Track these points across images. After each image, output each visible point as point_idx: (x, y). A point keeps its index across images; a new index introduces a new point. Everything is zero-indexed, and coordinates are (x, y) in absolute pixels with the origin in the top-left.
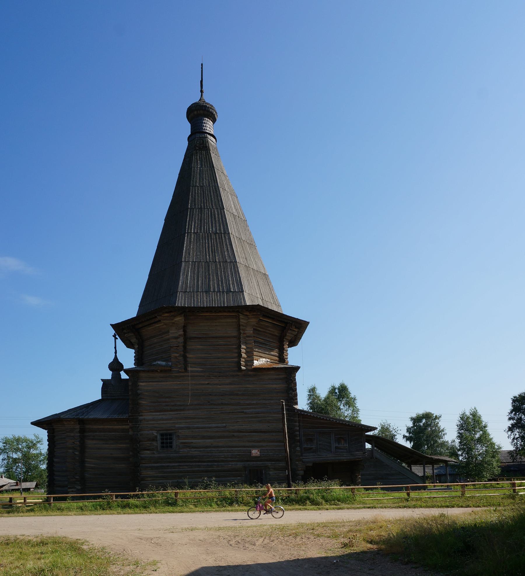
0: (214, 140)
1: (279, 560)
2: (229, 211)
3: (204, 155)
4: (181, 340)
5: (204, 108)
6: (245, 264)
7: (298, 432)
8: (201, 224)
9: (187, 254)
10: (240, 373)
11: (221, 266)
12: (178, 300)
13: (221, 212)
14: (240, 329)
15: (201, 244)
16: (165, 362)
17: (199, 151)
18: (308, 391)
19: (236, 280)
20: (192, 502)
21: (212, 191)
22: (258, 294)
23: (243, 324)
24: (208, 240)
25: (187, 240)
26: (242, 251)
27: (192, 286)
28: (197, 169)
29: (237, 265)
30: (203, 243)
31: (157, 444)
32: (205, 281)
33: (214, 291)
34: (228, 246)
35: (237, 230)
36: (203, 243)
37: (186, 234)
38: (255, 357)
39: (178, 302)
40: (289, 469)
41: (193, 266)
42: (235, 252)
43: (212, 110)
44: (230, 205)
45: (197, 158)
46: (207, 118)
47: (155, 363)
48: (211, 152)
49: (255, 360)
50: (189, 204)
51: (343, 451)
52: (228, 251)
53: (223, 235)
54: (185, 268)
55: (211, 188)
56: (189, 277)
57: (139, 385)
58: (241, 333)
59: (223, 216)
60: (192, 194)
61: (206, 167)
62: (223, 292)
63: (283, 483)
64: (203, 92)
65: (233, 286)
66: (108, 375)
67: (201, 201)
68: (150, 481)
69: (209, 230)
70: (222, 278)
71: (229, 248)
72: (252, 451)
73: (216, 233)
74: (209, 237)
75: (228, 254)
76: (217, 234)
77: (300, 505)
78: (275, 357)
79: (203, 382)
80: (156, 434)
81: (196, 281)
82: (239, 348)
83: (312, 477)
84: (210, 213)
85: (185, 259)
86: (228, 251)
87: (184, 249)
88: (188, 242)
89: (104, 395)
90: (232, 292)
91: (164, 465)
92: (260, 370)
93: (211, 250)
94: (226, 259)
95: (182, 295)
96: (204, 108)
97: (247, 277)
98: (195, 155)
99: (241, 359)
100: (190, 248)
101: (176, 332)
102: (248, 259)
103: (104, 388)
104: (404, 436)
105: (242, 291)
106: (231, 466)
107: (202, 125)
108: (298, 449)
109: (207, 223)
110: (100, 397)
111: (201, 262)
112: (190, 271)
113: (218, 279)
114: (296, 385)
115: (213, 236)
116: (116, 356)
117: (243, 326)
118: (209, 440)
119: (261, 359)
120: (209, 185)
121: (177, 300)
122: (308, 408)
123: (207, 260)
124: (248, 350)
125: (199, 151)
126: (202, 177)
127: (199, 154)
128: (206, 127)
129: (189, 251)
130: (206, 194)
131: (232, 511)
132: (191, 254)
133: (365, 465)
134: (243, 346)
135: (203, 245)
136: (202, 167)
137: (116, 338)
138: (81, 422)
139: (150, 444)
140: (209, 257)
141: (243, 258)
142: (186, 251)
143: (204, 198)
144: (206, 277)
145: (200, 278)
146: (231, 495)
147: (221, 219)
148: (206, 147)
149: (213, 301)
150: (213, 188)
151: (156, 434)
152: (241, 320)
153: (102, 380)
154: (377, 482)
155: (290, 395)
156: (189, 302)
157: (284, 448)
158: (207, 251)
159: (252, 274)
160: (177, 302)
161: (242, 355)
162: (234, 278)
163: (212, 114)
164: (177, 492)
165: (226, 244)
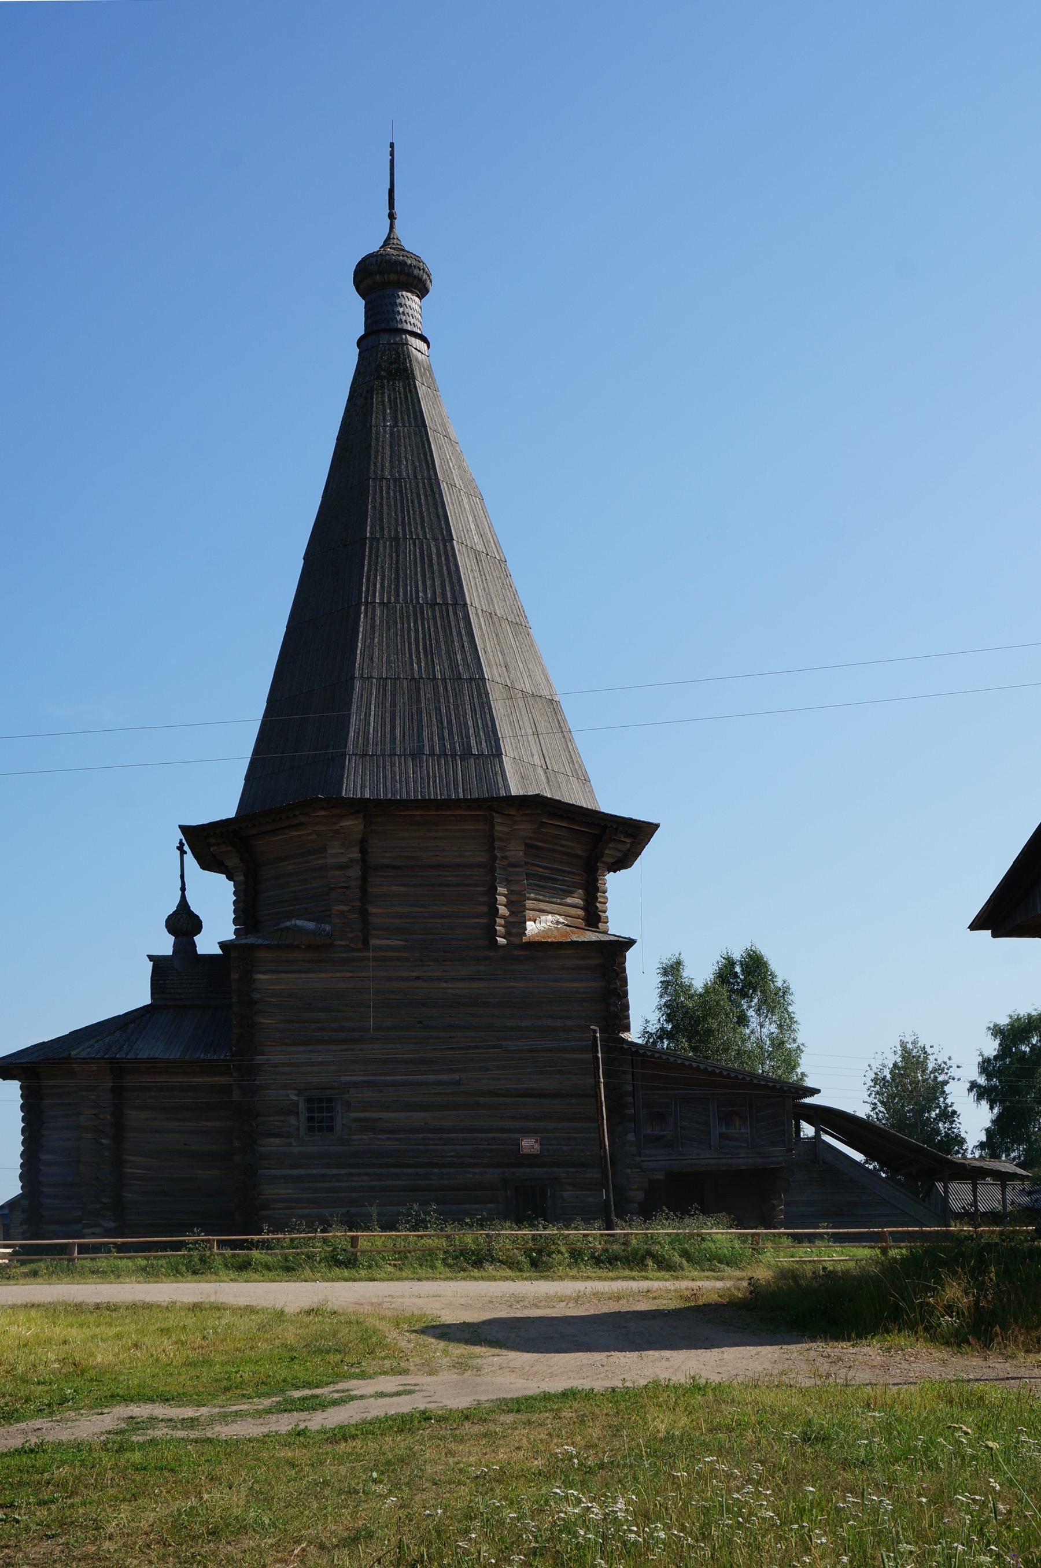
0: (422, 346)
1: (594, 1313)
2: (464, 542)
3: (400, 394)
4: (355, 872)
5: (399, 268)
6: (503, 682)
7: (632, 1098)
8: (397, 579)
9: (367, 660)
10: (492, 954)
11: (447, 690)
12: (347, 776)
13: (445, 547)
14: (494, 848)
15: (399, 632)
16: (314, 923)
17: (388, 382)
18: (661, 971)
19: (483, 725)
20: (389, 1260)
21: (422, 492)
22: (536, 757)
23: (501, 835)
24: (416, 623)
25: (365, 622)
26: (497, 646)
27: (379, 739)
28: (385, 431)
29: (485, 686)
30: (403, 631)
31: (298, 1122)
32: (411, 728)
33: (432, 754)
34: (465, 638)
35: (485, 591)
36: (403, 631)
37: (363, 608)
38: (529, 914)
39: (347, 781)
40: (608, 1186)
41: (381, 690)
42: (480, 654)
43: (420, 270)
44: (465, 524)
45: (383, 402)
46: (407, 291)
47: (288, 924)
48: (417, 382)
49: (530, 920)
50: (368, 528)
51: (738, 1144)
52: (463, 652)
53: (450, 608)
54: (362, 695)
55: (421, 485)
56: (372, 719)
57: (254, 980)
58: (497, 857)
59: (451, 558)
60: (374, 500)
61: (407, 425)
62: (454, 756)
63: (595, 1219)
64: (395, 219)
65: (476, 742)
66: (165, 945)
67: (397, 520)
68: (281, 1211)
69: (418, 597)
70: (450, 721)
71: (466, 644)
72: (522, 1140)
73: (434, 605)
74: (419, 614)
75: (465, 659)
76: (437, 608)
77: (631, 1269)
78: (575, 909)
79: (406, 974)
80: (295, 1098)
81: (388, 727)
82: (492, 892)
83: (664, 1208)
84: (418, 550)
85: (361, 672)
86: (463, 652)
87: (357, 646)
88: (369, 627)
89: (157, 996)
90: (476, 757)
91: (314, 1172)
92: (539, 947)
93: (423, 649)
94: (459, 670)
95: (355, 763)
96: (399, 268)
97: (508, 716)
98: (377, 394)
99: (496, 921)
100: (373, 643)
101: (342, 853)
102: (511, 666)
103: (157, 978)
104: (973, 1085)
105: (499, 755)
106: (471, 1176)
107: (393, 311)
108: (631, 1137)
109: (413, 576)
110: (147, 1000)
111: (399, 678)
112: (373, 702)
113: (442, 723)
114: (627, 983)
115: (428, 613)
116: (183, 896)
117: (501, 839)
118: (422, 1115)
119: (543, 918)
120: (416, 477)
121: (346, 776)
122: (659, 1020)
123: (413, 674)
124: (514, 898)
125: (388, 382)
126: (397, 453)
127: (389, 390)
128: (404, 315)
129: (371, 651)
130: (407, 500)
131: (483, 1279)
132: (375, 659)
133: (791, 1180)
134: (500, 890)
135: (403, 637)
136: (396, 425)
137: (183, 853)
138: (118, 1069)
139: (282, 1121)
140: (420, 667)
141: (500, 665)
142: (364, 650)
143: (403, 512)
144: (412, 719)
145: (398, 722)
146: (478, 1245)
147: (445, 568)
148: (406, 370)
149: (431, 779)
150: (424, 483)
151: (295, 1098)
152: (497, 828)
153: (151, 958)
154: (821, 1222)
155: (612, 1008)
156: (373, 781)
157: (598, 1135)
158: (414, 650)
159: (521, 706)
160: (345, 780)
161: (498, 910)
162: (480, 722)
163: (420, 279)
164: (357, 1237)
165: (459, 633)
